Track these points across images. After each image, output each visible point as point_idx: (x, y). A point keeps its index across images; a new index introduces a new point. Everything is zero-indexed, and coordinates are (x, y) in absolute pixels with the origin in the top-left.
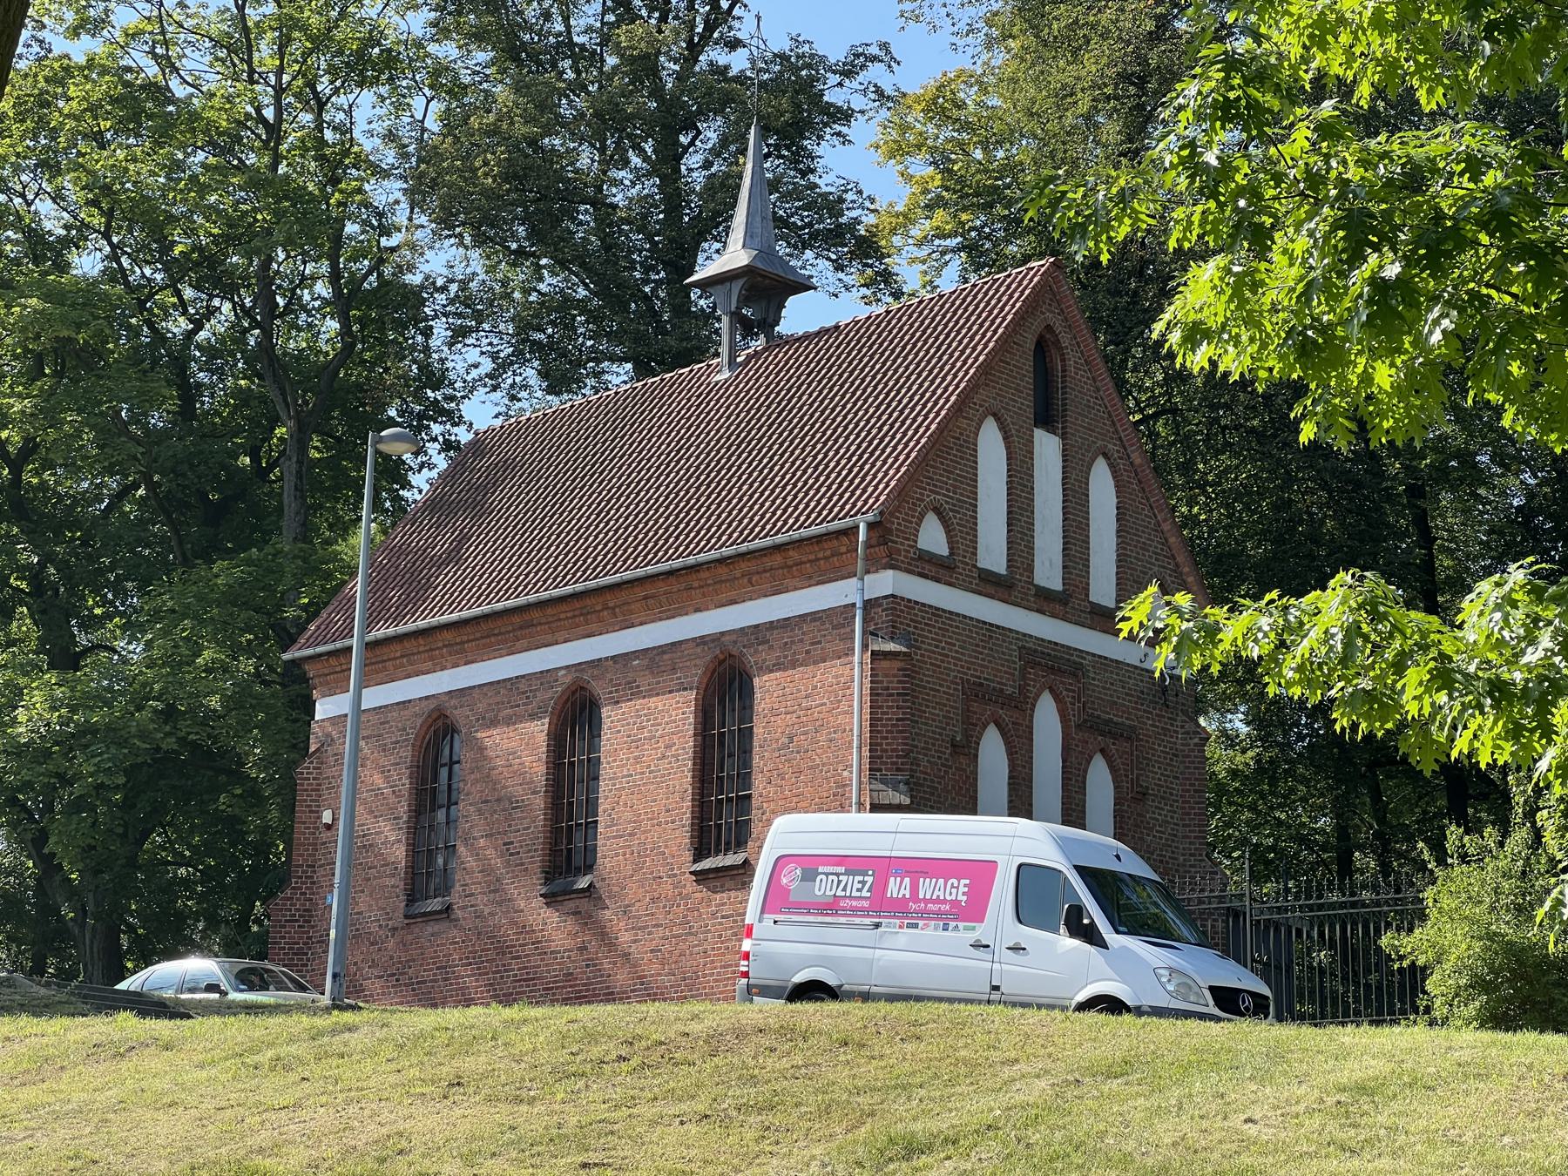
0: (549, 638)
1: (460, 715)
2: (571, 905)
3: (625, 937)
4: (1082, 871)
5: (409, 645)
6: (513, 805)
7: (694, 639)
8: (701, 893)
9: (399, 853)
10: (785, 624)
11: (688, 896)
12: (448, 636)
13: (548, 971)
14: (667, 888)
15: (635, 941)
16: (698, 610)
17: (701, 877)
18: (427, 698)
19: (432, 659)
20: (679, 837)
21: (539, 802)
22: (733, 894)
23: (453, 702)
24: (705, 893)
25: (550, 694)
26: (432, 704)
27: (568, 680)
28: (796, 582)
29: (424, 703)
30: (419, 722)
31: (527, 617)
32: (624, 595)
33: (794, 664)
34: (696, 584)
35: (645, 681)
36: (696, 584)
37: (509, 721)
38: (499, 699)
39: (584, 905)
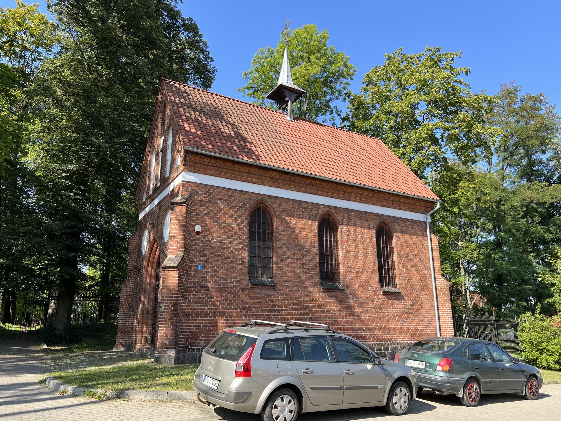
0: (315, 192)
1: (338, 217)
2: (334, 294)
3: (358, 310)
4: (435, 408)
5: (220, 163)
6: (303, 250)
7: (373, 213)
8: (384, 299)
9: (245, 255)
10: (403, 219)
11: (380, 299)
12: (274, 174)
13: (326, 318)
14: (372, 294)
15: (362, 312)
16: (373, 204)
17: (385, 293)
18: (256, 194)
19: (259, 179)
20: (375, 278)
21: (316, 251)
22: (395, 301)
23: (270, 200)
24: (386, 299)
25: (317, 212)
26: (259, 198)
27: (325, 210)
28: (404, 208)
29: (254, 195)
30: (252, 202)
31: (313, 182)
32: (353, 190)
33: (406, 233)
34: (377, 197)
35: (357, 221)
36: (377, 197)
37: (299, 217)
38: (293, 206)
39: (339, 295)
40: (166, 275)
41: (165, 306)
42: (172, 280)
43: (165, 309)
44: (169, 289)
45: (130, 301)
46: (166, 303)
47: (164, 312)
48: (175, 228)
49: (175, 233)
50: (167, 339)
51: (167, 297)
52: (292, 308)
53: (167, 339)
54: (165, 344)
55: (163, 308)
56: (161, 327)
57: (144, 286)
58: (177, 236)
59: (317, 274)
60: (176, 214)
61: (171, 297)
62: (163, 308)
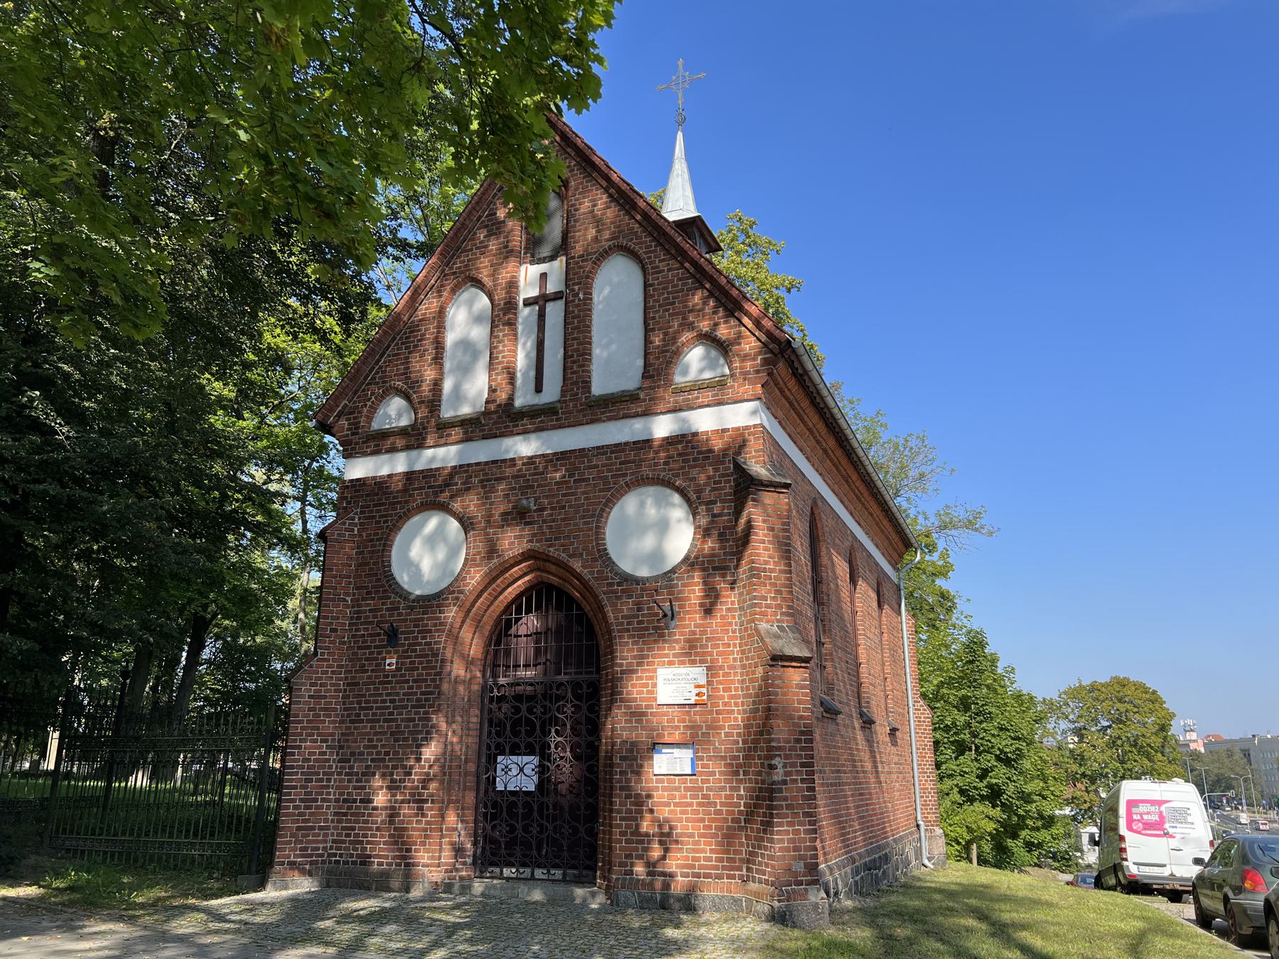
40: (780, 678)
41: (785, 766)
42: (796, 694)
43: (787, 774)
44: (791, 717)
45: (328, 725)
46: (787, 757)
47: (784, 782)
48: (766, 549)
49: (767, 563)
50: (801, 858)
51: (788, 741)
52: (359, 715)
53: (801, 858)
54: (795, 874)
55: (780, 771)
56: (781, 825)
57: (445, 687)
58: (771, 571)
59: (414, 453)
60: (765, 510)
61: (798, 741)
62: (780, 771)
